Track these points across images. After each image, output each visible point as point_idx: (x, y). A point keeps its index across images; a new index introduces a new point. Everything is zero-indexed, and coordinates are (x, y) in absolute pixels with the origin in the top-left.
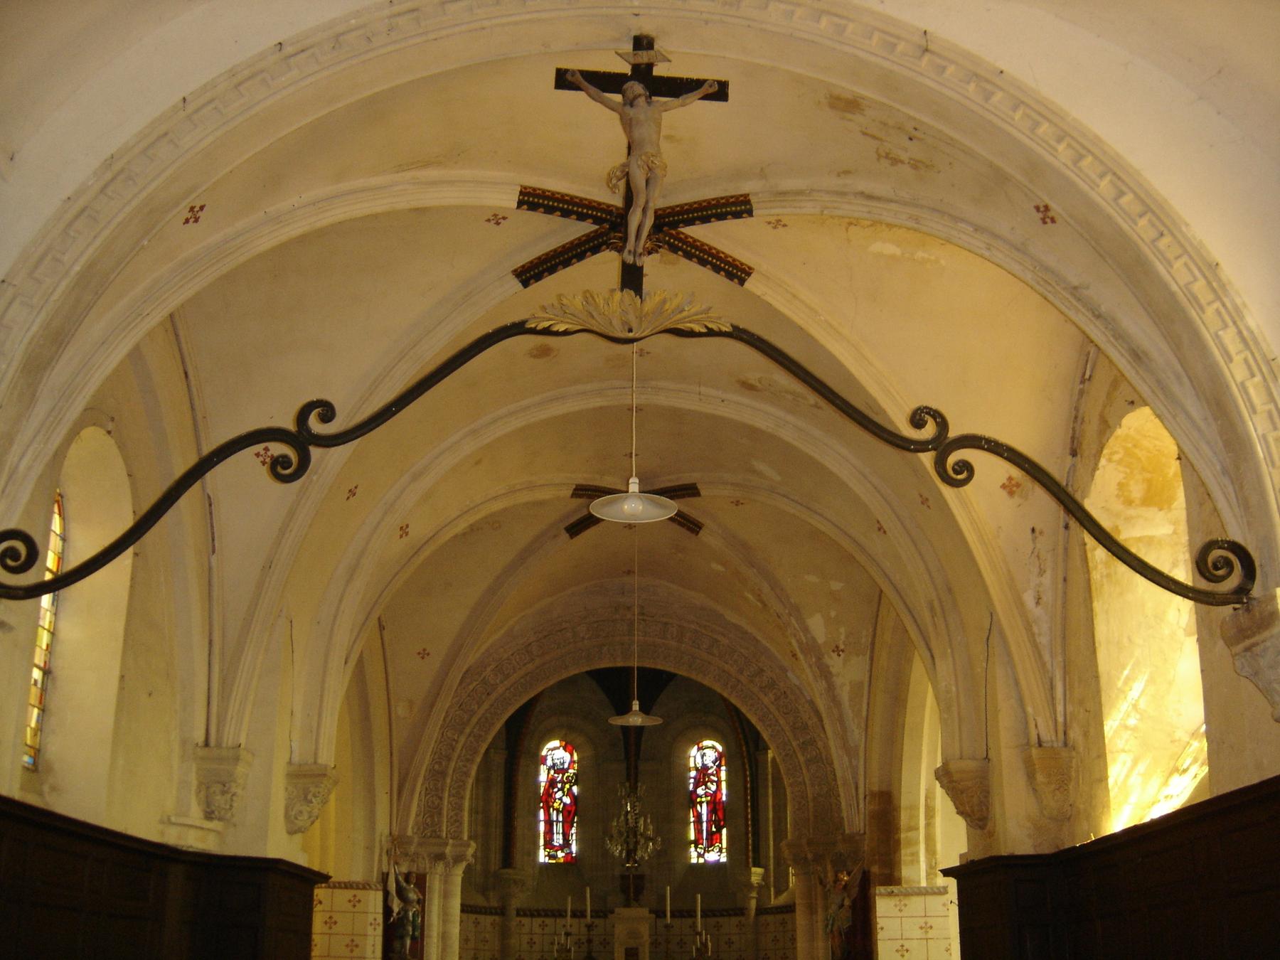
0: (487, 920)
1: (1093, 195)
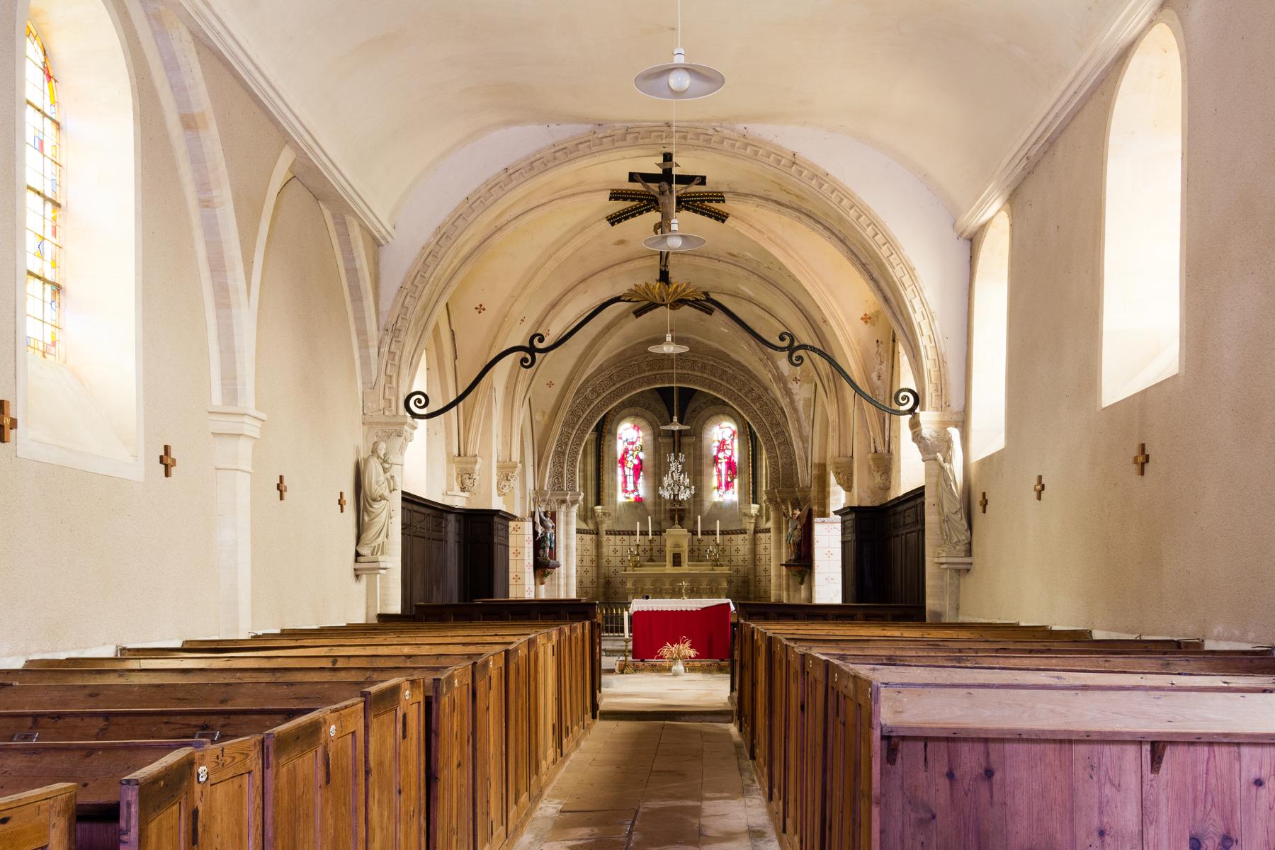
0: (588, 537)
1: (864, 234)
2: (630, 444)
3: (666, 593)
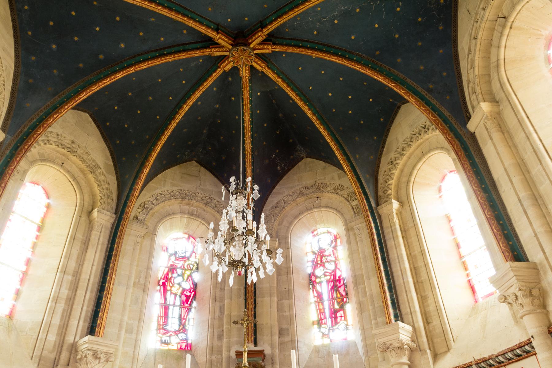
2: (178, 259)
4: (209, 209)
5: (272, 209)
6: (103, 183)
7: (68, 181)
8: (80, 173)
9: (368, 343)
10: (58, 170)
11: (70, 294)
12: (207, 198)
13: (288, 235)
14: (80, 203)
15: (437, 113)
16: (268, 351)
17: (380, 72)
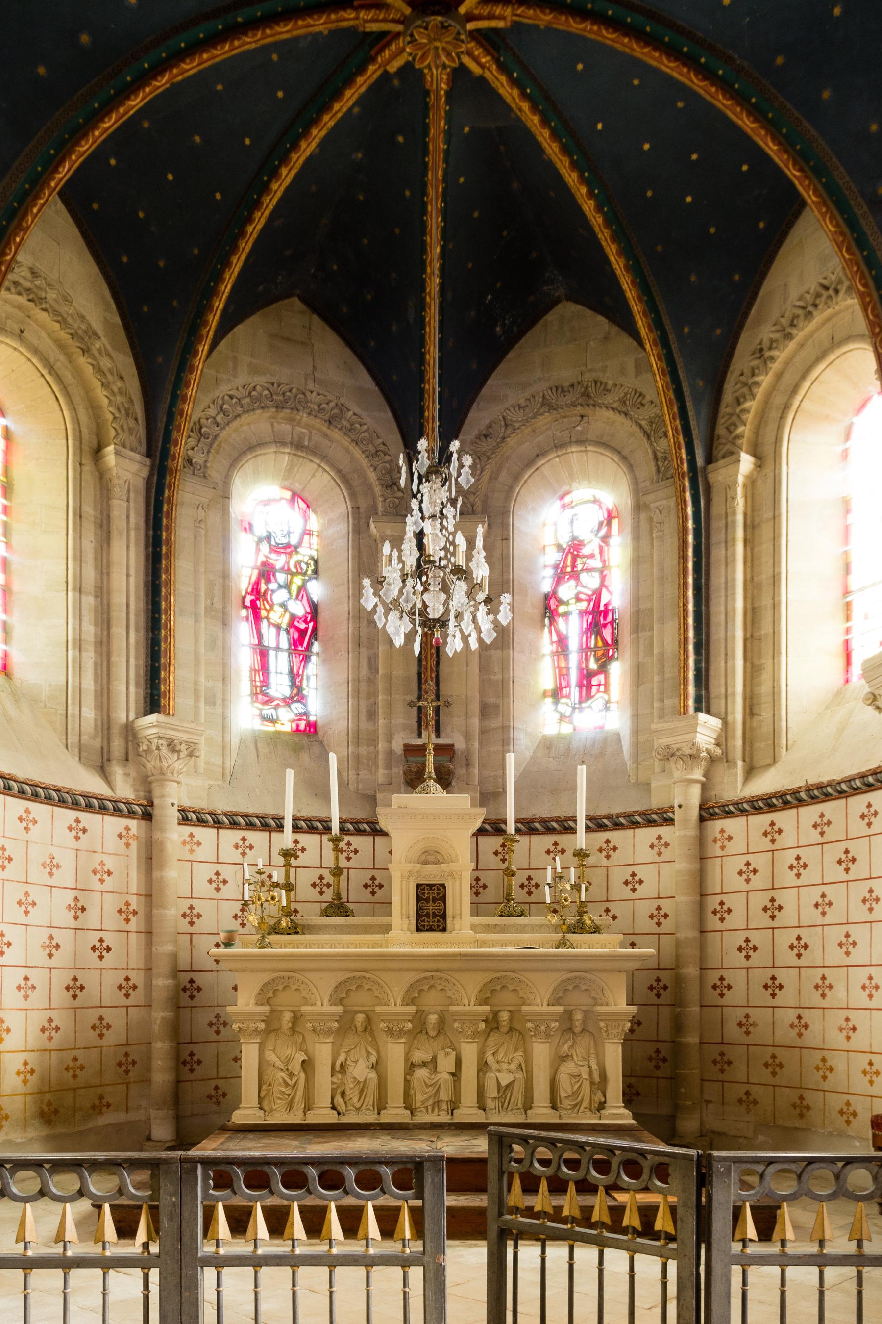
2: (277, 549)
3: (390, 1032)
4: (336, 434)
5: (477, 441)
6: (110, 378)
7: (39, 375)
8: (57, 351)
9: (642, 738)
10: (15, 349)
11: (99, 632)
12: (332, 404)
13: (509, 506)
14: (74, 429)
15: (873, 272)
16: (460, 745)
17: (773, 127)
